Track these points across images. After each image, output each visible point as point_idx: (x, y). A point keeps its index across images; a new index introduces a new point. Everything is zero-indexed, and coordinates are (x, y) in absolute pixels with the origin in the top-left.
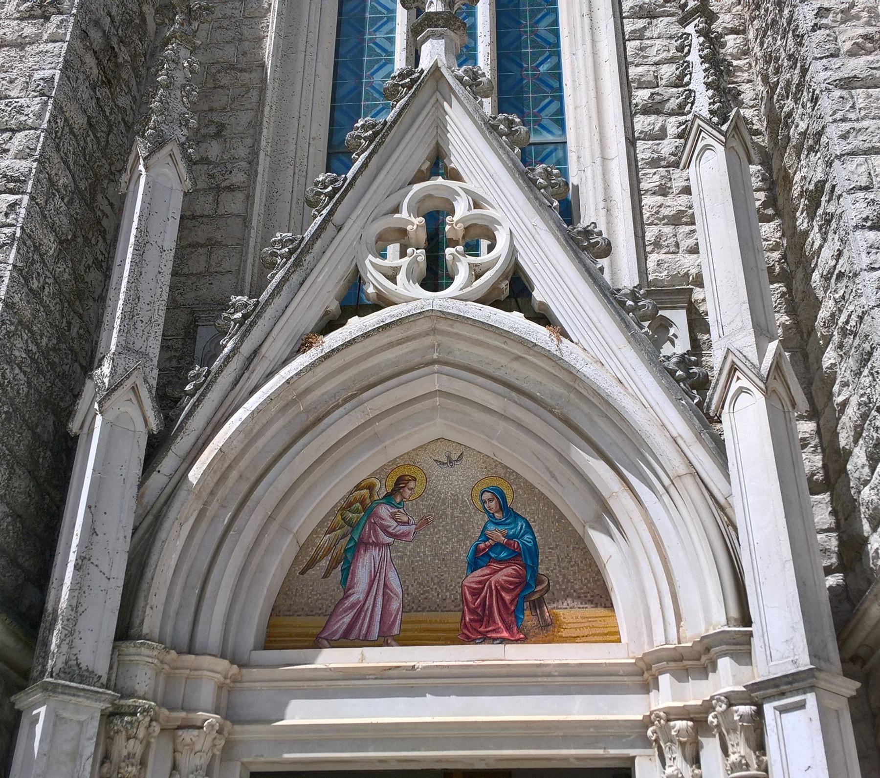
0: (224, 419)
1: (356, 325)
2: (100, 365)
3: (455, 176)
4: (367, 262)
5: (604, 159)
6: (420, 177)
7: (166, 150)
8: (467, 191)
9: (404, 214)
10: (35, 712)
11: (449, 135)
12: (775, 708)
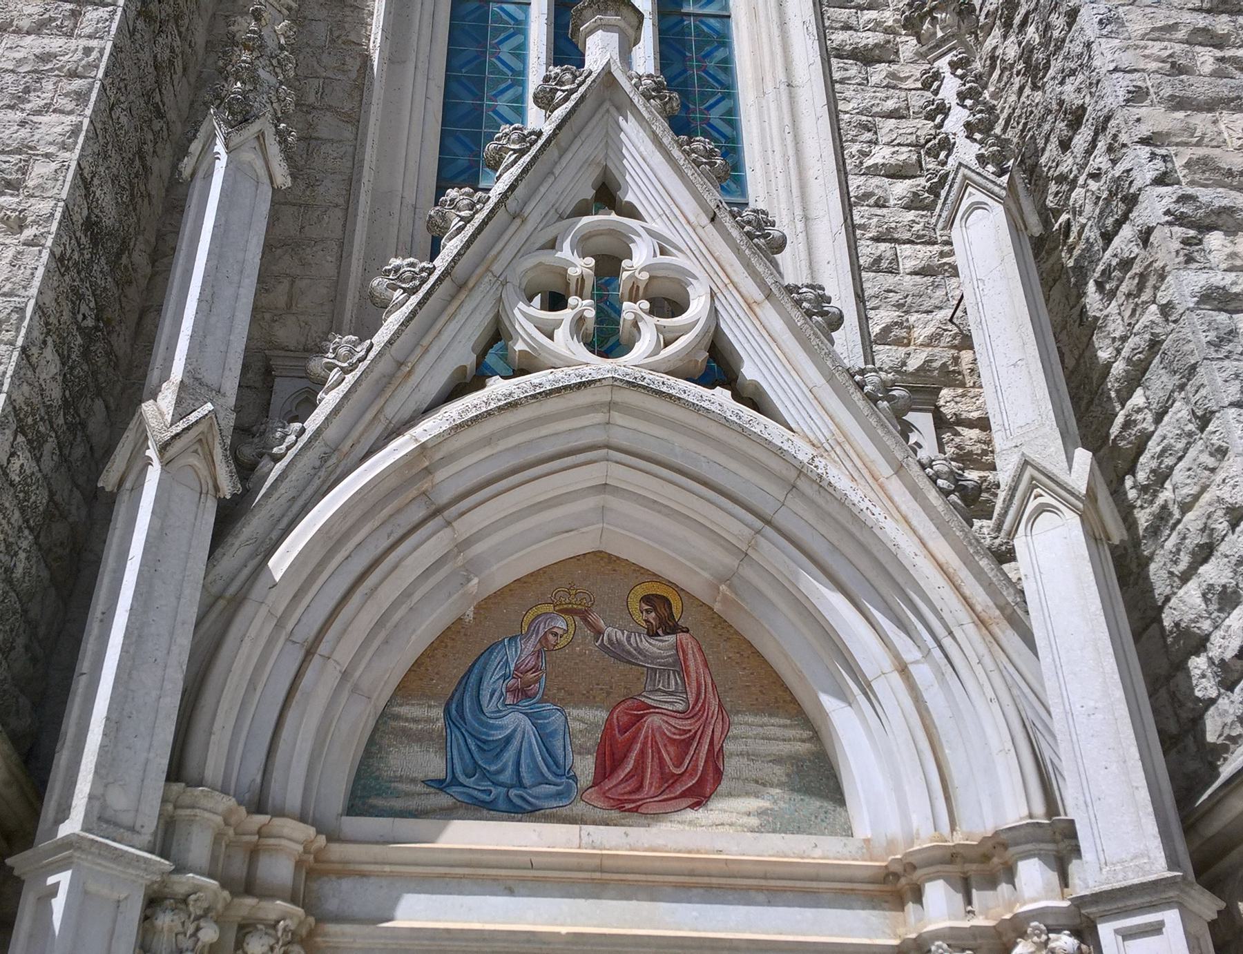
0: (325, 488)
1: (498, 388)
2: (154, 396)
3: (632, 212)
4: (516, 311)
5: (806, 219)
6: (582, 210)
7: (254, 128)
8: (649, 231)
9: (566, 252)
10: (51, 880)
11: (625, 161)
12: (1117, 931)
